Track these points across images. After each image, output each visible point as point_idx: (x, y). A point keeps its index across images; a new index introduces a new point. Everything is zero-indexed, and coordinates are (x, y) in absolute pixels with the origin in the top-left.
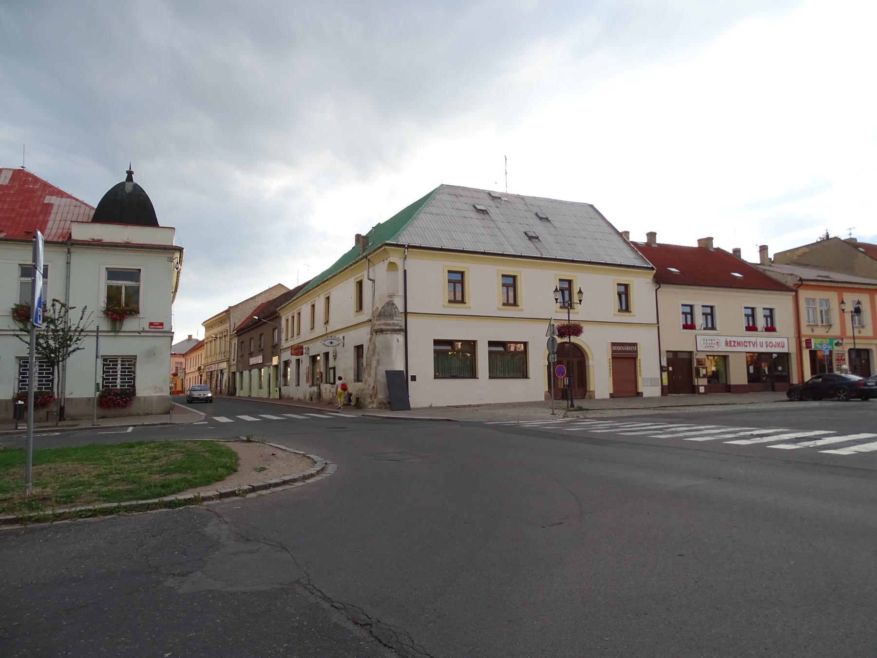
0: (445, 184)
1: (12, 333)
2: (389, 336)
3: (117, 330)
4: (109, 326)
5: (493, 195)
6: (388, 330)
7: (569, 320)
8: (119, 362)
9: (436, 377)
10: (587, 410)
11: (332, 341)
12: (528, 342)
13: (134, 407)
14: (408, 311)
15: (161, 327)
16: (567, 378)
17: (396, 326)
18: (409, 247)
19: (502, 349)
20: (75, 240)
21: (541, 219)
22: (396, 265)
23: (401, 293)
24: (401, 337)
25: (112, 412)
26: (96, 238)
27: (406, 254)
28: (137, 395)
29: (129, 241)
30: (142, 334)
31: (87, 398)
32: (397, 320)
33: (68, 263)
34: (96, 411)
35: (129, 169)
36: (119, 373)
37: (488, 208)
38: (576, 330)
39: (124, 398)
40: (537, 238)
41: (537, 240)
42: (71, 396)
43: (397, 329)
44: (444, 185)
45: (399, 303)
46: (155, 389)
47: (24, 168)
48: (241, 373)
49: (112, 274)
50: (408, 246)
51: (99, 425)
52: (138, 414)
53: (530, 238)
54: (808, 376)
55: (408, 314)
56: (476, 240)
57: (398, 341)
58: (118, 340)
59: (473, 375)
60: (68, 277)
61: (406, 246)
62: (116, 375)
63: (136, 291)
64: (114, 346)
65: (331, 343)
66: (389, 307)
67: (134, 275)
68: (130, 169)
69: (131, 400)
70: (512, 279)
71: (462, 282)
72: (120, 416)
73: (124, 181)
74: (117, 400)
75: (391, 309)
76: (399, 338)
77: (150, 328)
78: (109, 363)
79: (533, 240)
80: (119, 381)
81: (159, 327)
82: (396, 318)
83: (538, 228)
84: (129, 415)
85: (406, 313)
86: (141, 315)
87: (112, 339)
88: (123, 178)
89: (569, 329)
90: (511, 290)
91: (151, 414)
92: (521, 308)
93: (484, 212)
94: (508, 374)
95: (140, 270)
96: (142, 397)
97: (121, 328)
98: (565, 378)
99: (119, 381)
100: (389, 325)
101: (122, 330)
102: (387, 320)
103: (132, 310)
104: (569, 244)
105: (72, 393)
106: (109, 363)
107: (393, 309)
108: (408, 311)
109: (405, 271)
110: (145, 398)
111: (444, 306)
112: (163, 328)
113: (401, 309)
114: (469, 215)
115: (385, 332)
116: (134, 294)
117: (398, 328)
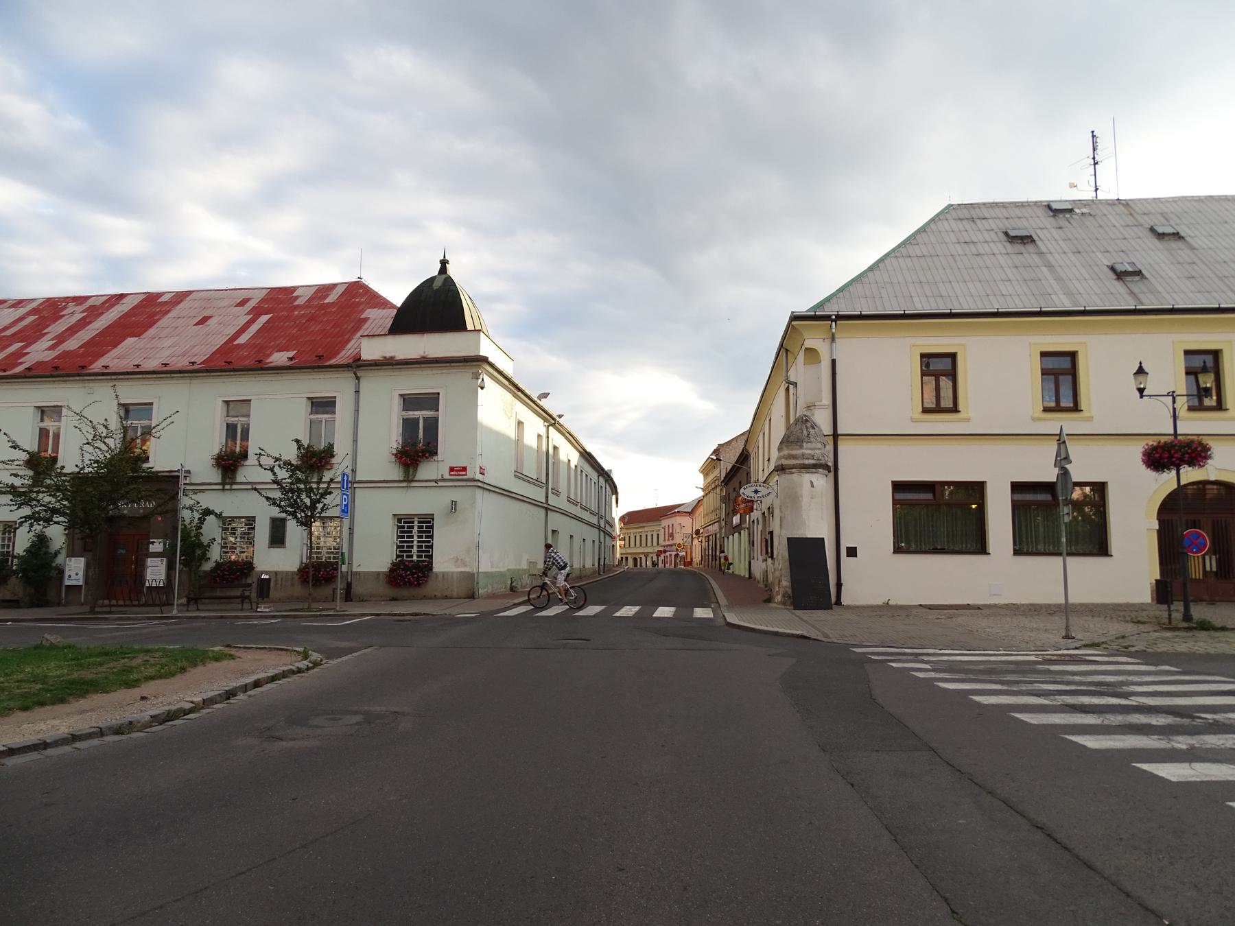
0: (956, 203)
1: (249, 487)
2: (795, 477)
3: (410, 478)
4: (401, 474)
5: (1054, 206)
6: (794, 467)
7: (1175, 434)
8: (416, 523)
9: (898, 550)
10: (1223, 629)
11: (758, 488)
12: (1107, 482)
13: (431, 587)
14: (839, 432)
15: (464, 473)
16: (1214, 557)
17: (808, 459)
18: (840, 317)
19: (929, 496)
20: (364, 361)
21: (1161, 236)
22: (819, 354)
23: (827, 400)
24: (821, 481)
25: (405, 592)
26: (388, 355)
27: (834, 330)
28: (434, 570)
29: (425, 355)
30: (440, 484)
31: (376, 572)
32: (811, 449)
33: (357, 392)
34: (383, 589)
35: (443, 258)
36: (415, 538)
37: (1039, 232)
38: (1187, 453)
39: (416, 573)
40: (1139, 273)
41: (1137, 278)
42: (359, 570)
43: (809, 465)
44: (952, 205)
45: (822, 419)
46: (456, 562)
47: (361, 279)
48: (728, 538)
49: (410, 402)
50: (836, 316)
51: (346, 611)
52: (435, 597)
53: (1120, 275)
54: (1201, 577)
55: (840, 437)
56: (989, 292)
57: (812, 486)
58: (412, 492)
59: (980, 546)
60: (357, 411)
61: (834, 317)
62: (412, 542)
63: (435, 421)
64: (415, 502)
65: (756, 492)
66: (798, 427)
67: (431, 401)
68: (444, 257)
69: (427, 577)
70: (949, 360)
71: (1073, 373)
72: (413, 598)
73: (436, 274)
74: (406, 576)
75: (801, 429)
76: (814, 481)
77: (450, 475)
78: (404, 522)
79: (1129, 278)
80: (415, 549)
81: (461, 473)
82: (809, 445)
83: (1149, 256)
84: (425, 597)
85: (835, 436)
86: (440, 457)
87: (404, 491)
88: (434, 270)
89: (1169, 452)
90: (1065, 381)
91: (451, 598)
92: (1088, 415)
93: (1026, 240)
94: (916, 544)
95: (438, 394)
96: (440, 572)
97: (414, 477)
98: (1207, 558)
99: (415, 549)
100: (794, 457)
101: (416, 479)
102: (792, 449)
103: (430, 450)
104: (1220, 278)
105: (360, 565)
106: (404, 522)
107: (805, 429)
108: (839, 432)
109: (834, 362)
110: (444, 574)
111: (913, 420)
112: (466, 475)
113: (827, 429)
114: (1186, 258)
115: (787, 471)
116: (432, 426)
117: (812, 462)
